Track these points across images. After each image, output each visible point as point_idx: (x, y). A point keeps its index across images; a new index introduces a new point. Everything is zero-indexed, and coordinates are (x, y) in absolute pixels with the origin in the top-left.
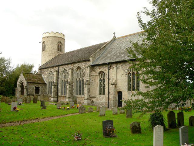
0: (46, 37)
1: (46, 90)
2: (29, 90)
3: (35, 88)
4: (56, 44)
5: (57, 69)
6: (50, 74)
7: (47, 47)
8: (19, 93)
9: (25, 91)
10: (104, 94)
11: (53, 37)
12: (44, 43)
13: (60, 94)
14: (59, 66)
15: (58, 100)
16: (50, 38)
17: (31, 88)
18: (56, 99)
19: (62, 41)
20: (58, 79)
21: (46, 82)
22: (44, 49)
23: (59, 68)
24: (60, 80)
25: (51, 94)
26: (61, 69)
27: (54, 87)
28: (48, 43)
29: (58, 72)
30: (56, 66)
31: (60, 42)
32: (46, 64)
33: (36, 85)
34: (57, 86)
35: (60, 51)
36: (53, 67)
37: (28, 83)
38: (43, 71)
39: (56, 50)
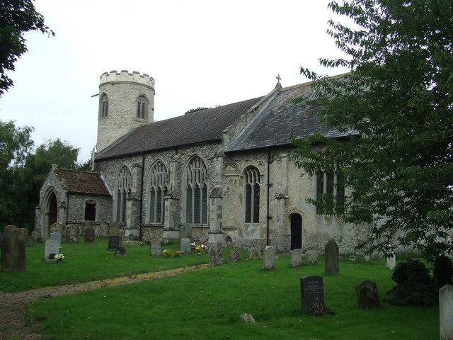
0: (108, 83)
2: (71, 211)
3: (84, 206)
4: (134, 100)
5: (140, 161)
6: (121, 172)
8: (44, 218)
9: (61, 212)
11: (126, 82)
13: (147, 220)
15: (141, 235)
16: (121, 85)
18: (136, 233)
19: (147, 94)
20: (142, 184)
21: (113, 193)
22: (104, 111)
23: (144, 159)
24: (147, 188)
26: (150, 160)
27: (134, 205)
31: (143, 96)
32: (111, 148)
34: (139, 202)
38: (103, 165)
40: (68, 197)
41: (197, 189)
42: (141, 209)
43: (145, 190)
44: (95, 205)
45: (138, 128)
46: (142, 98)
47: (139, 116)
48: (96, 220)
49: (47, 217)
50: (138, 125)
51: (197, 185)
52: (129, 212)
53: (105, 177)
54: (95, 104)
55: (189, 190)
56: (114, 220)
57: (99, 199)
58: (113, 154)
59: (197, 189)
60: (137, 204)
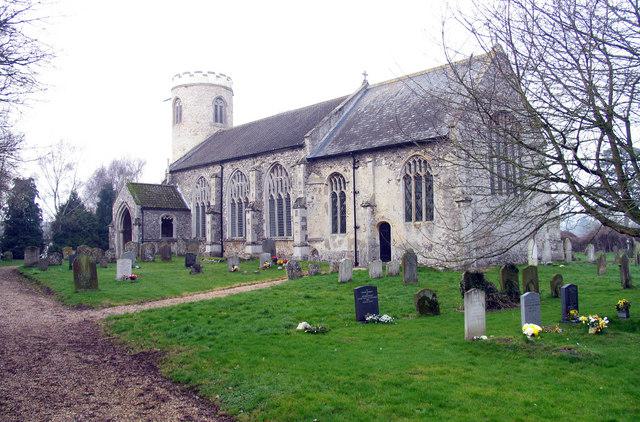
0: (181, 86)
2: (147, 228)
3: (160, 223)
5: (217, 169)
7: (185, 113)
8: (119, 237)
9: (135, 230)
10: (343, 230)
11: (201, 84)
13: (228, 234)
14: (222, 162)
15: (223, 251)
18: (217, 248)
19: (224, 94)
21: (191, 206)
22: (178, 117)
24: (227, 200)
25: (204, 235)
26: (228, 169)
28: (187, 100)
30: (213, 164)
32: (187, 158)
33: (163, 214)
34: (218, 214)
35: (221, 122)
36: (206, 165)
37: (143, 209)
38: (179, 176)
41: (240, 203)
42: (222, 223)
45: (216, 135)
47: (216, 121)
48: (174, 236)
49: (121, 235)
50: (217, 130)
51: (240, 200)
52: (208, 227)
54: (169, 108)
55: (272, 201)
56: (194, 235)
58: (190, 164)
60: (217, 217)
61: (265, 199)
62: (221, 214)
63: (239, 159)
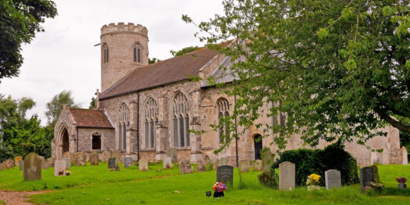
1: (114, 141)
3: (91, 138)
5: (135, 97)
6: (121, 108)
8: (59, 150)
12: (106, 46)
13: (143, 147)
17: (83, 137)
19: (142, 41)
20: (138, 117)
21: (115, 125)
23: (139, 96)
24: (142, 119)
27: (132, 134)
29: (138, 104)
30: (132, 93)
33: (94, 132)
35: (139, 61)
36: (127, 94)
38: (106, 102)
39: (132, 61)
40: (77, 130)
41: (181, 119)
42: (138, 137)
43: (141, 122)
44: (100, 136)
46: (137, 46)
47: (135, 60)
51: (181, 116)
53: (108, 113)
55: (175, 120)
57: (104, 131)
59: (181, 119)
60: (135, 133)
61: (171, 118)
62: (138, 131)
63: (150, 89)
